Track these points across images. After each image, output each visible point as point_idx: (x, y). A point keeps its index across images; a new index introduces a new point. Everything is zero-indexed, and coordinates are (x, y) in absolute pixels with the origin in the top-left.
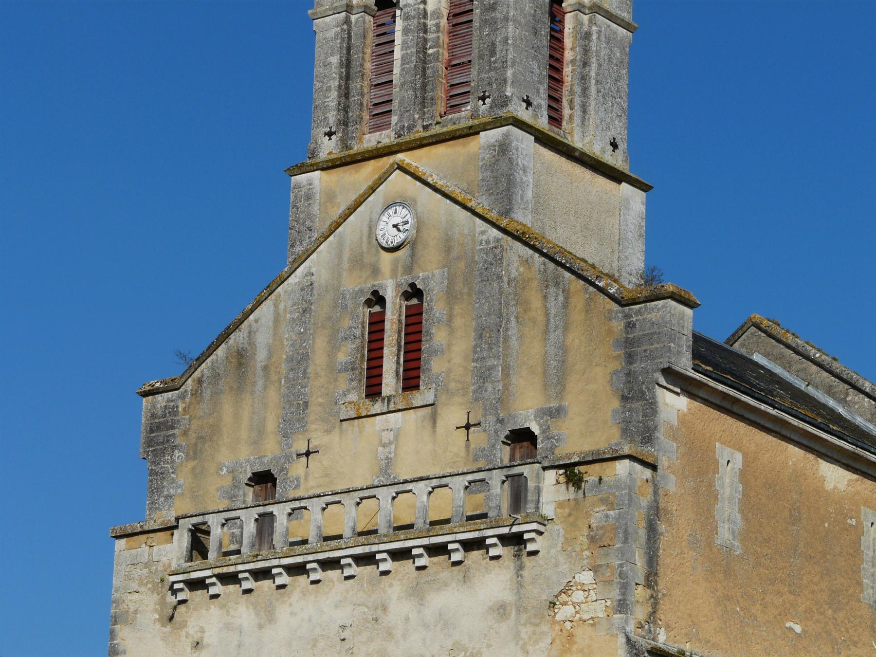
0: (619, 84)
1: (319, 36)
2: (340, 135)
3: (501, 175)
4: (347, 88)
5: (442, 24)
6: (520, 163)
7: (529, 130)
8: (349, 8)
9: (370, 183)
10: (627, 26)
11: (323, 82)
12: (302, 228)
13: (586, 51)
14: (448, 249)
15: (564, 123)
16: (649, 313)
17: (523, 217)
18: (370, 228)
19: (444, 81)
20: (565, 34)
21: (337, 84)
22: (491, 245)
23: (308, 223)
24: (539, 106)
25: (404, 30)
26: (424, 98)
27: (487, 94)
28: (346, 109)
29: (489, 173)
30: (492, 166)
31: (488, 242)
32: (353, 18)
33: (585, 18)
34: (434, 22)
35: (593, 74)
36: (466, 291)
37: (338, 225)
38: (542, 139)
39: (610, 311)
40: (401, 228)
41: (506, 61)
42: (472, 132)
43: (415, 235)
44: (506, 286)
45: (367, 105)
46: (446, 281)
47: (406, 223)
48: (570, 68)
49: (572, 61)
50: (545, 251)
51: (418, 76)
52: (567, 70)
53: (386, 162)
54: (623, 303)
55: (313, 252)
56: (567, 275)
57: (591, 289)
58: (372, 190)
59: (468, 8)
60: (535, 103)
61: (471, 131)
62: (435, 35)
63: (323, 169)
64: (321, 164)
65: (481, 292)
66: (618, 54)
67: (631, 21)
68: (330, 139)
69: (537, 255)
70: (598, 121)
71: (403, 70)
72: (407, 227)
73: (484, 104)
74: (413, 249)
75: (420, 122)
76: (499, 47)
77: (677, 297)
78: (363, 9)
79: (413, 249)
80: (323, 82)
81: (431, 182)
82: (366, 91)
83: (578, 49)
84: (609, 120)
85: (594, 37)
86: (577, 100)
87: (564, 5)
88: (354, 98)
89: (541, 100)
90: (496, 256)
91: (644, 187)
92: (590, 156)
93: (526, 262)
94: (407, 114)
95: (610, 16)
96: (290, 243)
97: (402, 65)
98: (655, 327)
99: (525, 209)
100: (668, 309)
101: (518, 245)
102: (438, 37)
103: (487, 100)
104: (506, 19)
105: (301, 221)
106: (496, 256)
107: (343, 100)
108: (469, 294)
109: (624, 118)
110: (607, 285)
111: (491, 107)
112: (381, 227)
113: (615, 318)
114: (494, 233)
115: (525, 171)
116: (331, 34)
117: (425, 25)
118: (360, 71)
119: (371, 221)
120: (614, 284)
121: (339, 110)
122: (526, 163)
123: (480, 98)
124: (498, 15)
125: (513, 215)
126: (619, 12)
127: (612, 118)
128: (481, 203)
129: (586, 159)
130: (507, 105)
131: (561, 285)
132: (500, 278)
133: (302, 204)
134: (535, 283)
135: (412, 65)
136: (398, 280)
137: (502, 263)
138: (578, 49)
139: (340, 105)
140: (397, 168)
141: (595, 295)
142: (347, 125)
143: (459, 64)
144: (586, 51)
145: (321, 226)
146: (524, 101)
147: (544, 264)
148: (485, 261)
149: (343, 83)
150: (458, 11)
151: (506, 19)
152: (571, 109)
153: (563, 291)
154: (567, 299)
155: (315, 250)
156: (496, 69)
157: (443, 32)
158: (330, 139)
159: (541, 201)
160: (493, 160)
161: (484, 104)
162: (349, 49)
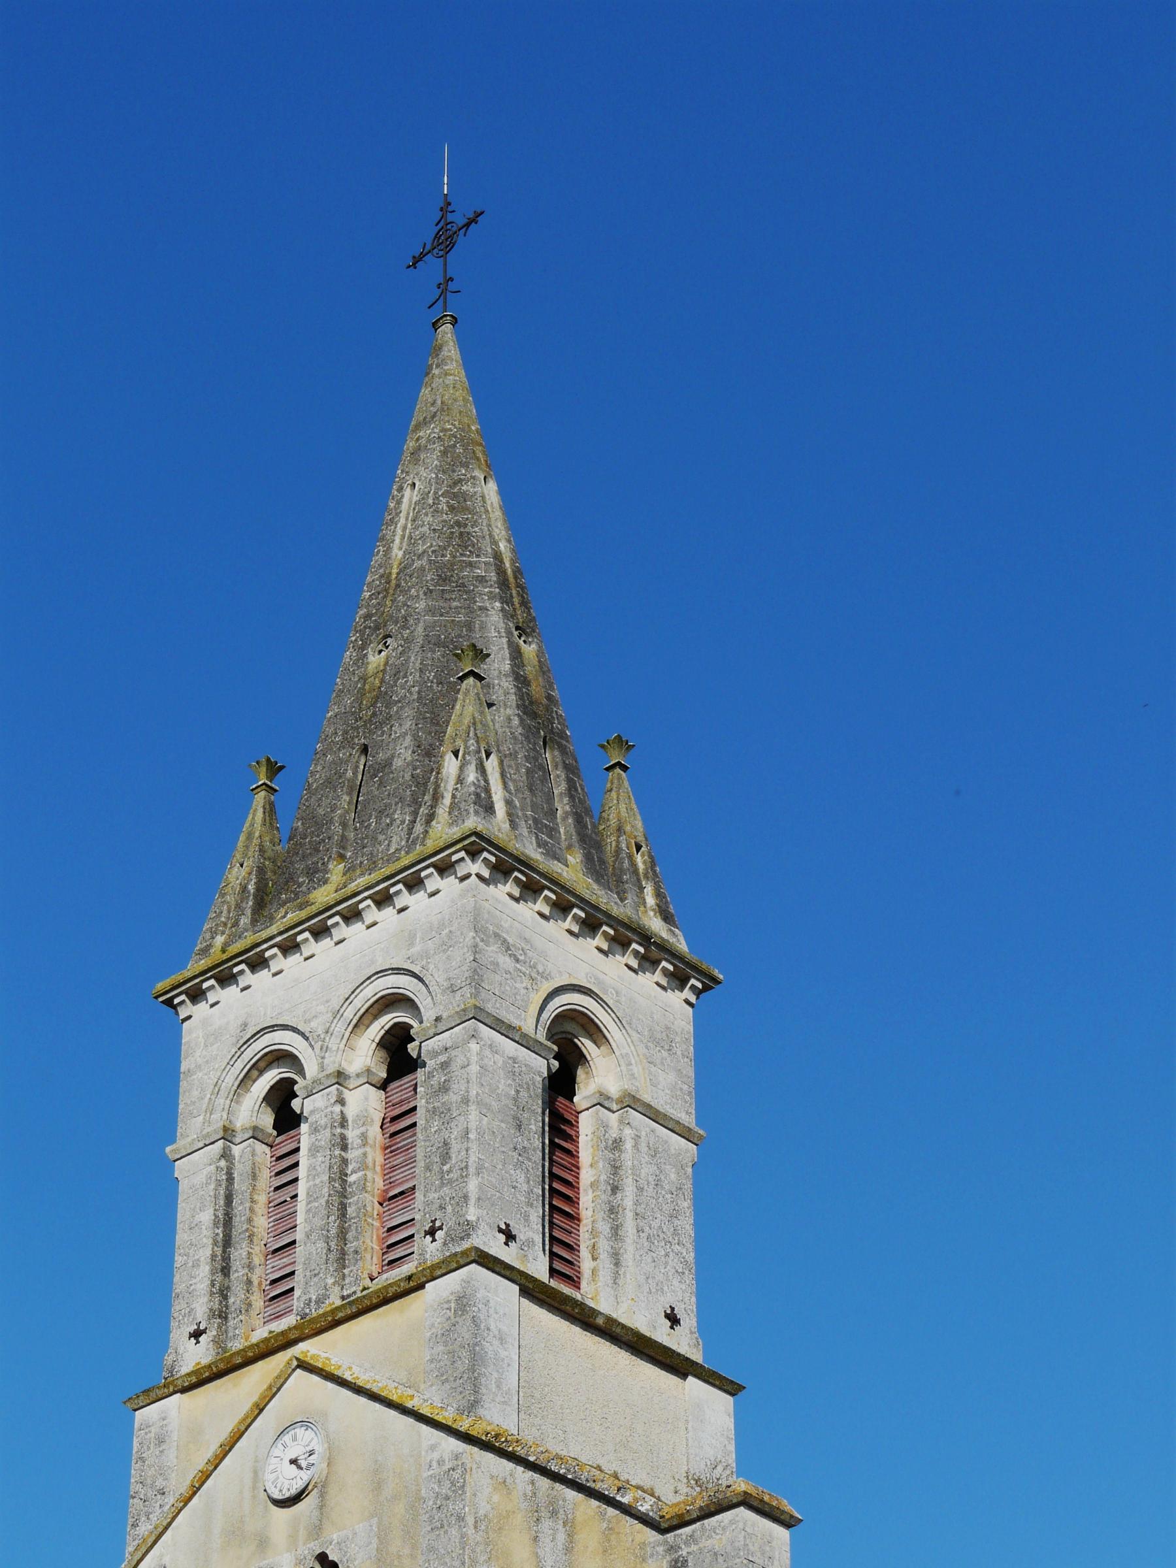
0: (676, 1222)
1: (183, 1186)
2: (214, 1333)
3: (466, 1362)
4: (226, 1258)
5: (371, 1134)
6: (492, 1327)
7: (508, 1273)
8: (228, 1134)
9: (255, 1398)
10: (686, 1134)
11: (187, 1255)
12: (150, 1493)
13: (616, 1168)
14: (378, 1486)
15: (584, 1284)
16: (710, 1537)
17: (497, 1416)
18: (256, 1473)
19: (377, 1224)
20: (580, 1145)
21: (209, 1252)
22: (448, 1466)
23: (160, 1483)
24: (530, 1243)
25: (310, 1150)
26: (343, 1253)
27: (438, 1224)
28: (224, 1293)
29: (441, 1348)
30: (447, 1335)
31: (440, 1462)
32: (236, 1150)
33: (613, 1118)
34: (358, 1132)
35: (629, 1203)
36: (407, 1551)
37: (205, 1476)
38: (531, 1290)
39: (643, 1545)
40: (303, 1464)
41: (467, 1167)
42: (413, 1286)
43: (325, 1472)
44: (470, 1531)
45: (260, 1284)
46: (375, 1541)
47: (311, 1453)
48: (590, 1196)
49: (592, 1185)
50: (532, 1459)
51: (332, 1218)
52: (586, 1200)
53: (280, 1360)
54: (664, 1525)
55: (166, 1528)
56: (571, 1494)
57: (611, 1512)
58: (260, 1409)
59: (411, 1105)
60: (521, 1237)
61: (412, 1284)
62: (361, 1151)
63: (184, 1390)
64: (179, 1382)
65: (431, 1549)
66: (673, 1176)
67: (693, 1125)
68: (198, 1342)
69: (520, 1469)
70: (642, 1279)
71: (308, 1211)
72: (312, 1459)
73: (434, 1240)
74: (322, 1495)
75: (337, 1289)
76: (455, 1147)
77: (755, 1504)
78: (250, 1134)
79: (322, 1495)
80: (187, 1255)
81: (349, 1378)
82: (257, 1260)
83: (601, 1165)
84: (660, 1277)
85: (628, 1145)
86: (604, 1246)
87: (575, 1099)
88: (238, 1273)
89: (532, 1230)
90: (455, 1482)
91: (731, 1388)
92: (624, 1326)
93: (503, 1484)
94: (316, 1279)
95: (655, 1116)
96: (131, 1521)
97: (308, 1204)
98: (720, 1560)
99: (505, 1403)
100: (741, 1525)
101: (490, 1457)
102: (365, 1154)
103: (439, 1235)
104: (466, 1101)
105: (149, 1481)
106: (455, 1482)
107: (219, 1277)
108: (413, 1557)
109: (689, 1278)
110: (636, 1500)
111: (445, 1244)
112: (272, 1467)
113: (652, 1555)
114: (453, 1444)
115: (502, 1340)
116: (201, 1178)
117: (343, 1138)
118: (247, 1230)
119: (256, 1461)
120: (648, 1497)
121: (212, 1294)
122: (505, 1329)
123: (427, 1233)
124: (453, 1097)
125: (481, 1412)
126: (671, 1111)
127: (666, 1274)
128: (427, 1400)
129: (618, 1330)
130: (469, 1235)
131: (561, 1515)
132: (461, 1518)
133: (150, 1455)
134: (519, 1519)
135: (323, 1201)
136: (299, 1552)
137: (464, 1492)
138: (601, 1165)
139: (213, 1285)
140: (298, 1366)
141: (618, 1522)
142: (226, 1318)
143: (402, 1193)
144: (616, 1168)
145: (179, 1484)
146: (500, 1231)
147: (533, 1483)
148: (438, 1495)
149: (219, 1251)
150: (397, 1112)
151: (466, 1101)
152: (594, 1259)
153: (565, 1524)
154: (570, 1536)
155: (170, 1524)
156: (450, 1182)
157: (373, 1146)
158: (198, 1342)
159: (537, 1395)
160: (447, 1326)
161: (434, 1240)
162: (229, 1199)
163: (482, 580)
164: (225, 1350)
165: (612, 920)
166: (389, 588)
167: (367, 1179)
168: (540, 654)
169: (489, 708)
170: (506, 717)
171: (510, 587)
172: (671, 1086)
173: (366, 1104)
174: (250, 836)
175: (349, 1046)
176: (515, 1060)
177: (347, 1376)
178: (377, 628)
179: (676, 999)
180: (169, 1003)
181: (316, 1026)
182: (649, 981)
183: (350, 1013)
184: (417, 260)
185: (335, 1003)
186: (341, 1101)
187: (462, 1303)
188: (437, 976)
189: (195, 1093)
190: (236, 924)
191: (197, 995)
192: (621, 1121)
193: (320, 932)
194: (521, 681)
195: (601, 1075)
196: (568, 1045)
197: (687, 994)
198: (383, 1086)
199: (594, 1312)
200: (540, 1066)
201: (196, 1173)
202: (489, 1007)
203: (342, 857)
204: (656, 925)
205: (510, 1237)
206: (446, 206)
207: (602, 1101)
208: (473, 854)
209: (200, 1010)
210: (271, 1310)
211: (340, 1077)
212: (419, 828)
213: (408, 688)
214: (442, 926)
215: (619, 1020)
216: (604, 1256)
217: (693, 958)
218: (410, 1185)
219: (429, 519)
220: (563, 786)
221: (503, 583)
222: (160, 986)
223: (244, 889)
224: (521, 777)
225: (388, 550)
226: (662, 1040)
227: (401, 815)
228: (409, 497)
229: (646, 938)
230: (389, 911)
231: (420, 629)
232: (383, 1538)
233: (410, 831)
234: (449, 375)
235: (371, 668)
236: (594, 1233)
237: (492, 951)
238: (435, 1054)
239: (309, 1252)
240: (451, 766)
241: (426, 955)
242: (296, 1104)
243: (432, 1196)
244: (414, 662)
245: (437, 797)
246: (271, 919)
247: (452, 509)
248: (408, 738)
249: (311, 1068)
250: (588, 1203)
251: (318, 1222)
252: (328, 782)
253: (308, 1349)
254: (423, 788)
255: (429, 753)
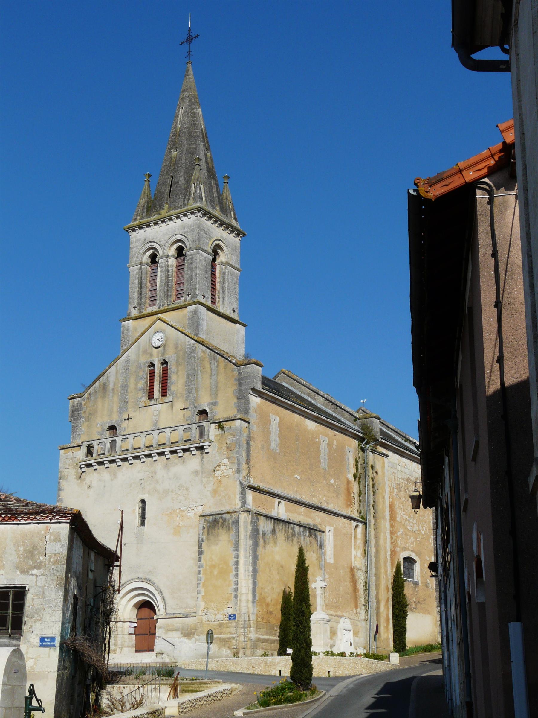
1: (131, 273)
4: (141, 291)
10: (238, 270)
13: (224, 278)
14: (176, 348)
15: (216, 303)
17: (203, 336)
23: (128, 339)
24: (208, 298)
30: (191, 318)
31: (190, 345)
32: (143, 267)
33: (224, 267)
35: (226, 286)
38: (209, 309)
39: (233, 368)
42: (184, 307)
58: (150, 327)
63: (133, 320)
65: (188, 362)
74: (164, 347)
76: (194, 277)
79: (164, 347)
85: (227, 273)
86: (221, 296)
88: (143, 295)
89: (209, 295)
90: (193, 350)
91: (244, 325)
93: (204, 352)
95: (232, 266)
104: (196, 267)
106: (193, 350)
109: (237, 302)
116: (135, 273)
117: (168, 269)
128: (188, 331)
133: (125, 332)
134: (207, 359)
144: (224, 278)
145: (132, 339)
151: (196, 267)
163: (198, 136)
164: (141, 312)
165: (226, 224)
166: (176, 135)
167: (173, 279)
168: (211, 154)
169: (200, 173)
170: (205, 172)
171: (205, 138)
172: (234, 260)
173: (172, 262)
174: (144, 193)
175: (170, 249)
176: (206, 257)
177: (170, 323)
178: (174, 145)
179: (237, 239)
180: (127, 231)
181: (162, 243)
182: (232, 236)
183: (170, 242)
184: (182, 43)
185: (167, 239)
186: (168, 261)
187: (195, 312)
188: (190, 238)
189: (133, 253)
190: (142, 215)
191: (134, 230)
192: (225, 268)
193: (163, 222)
194: (207, 163)
195: (222, 258)
196: (216, 251)
197: (239, 238)
198: (176, 258)
199: (220, 312)
200: (211, 258)
201: (134, 270)
202: (202, 247)
203: (167, 203)
204: (234, 223)
205: (204, 297)
206: (190, 31)
207: (222, 263)
208: (199, 211)
209: (134, 234)
210: (150, 303)
211: (168, 256)
212: (186, 202)
213: (183, 163)
214: (191, 226)
215: (226, 246)
216: (221, 298)
217: (241, 230)
218: (182, 281)
219: (186, 119)
220: (215, 190)
221: (203, 137)
222: (125, 227)
223: (144, 206)
224: (207, 189)
225: (176, 124)
226: (234, 249)
227: (182, 197)
228: (181, 111)
229: (232, 227)
230: (179, 220)
231: (185, 149)
232: (178, 358)
233: (184, 202)
234: (191, 79)
235: (173, 155)
236: (219, 292)
237: (202, 233)
238: (189, 255)
239: (159, 293)
240: (193, 187)
241: (187, 232)
242: (157, 260)
243: (189, 287)
244: (184, 157)
245: (190, 195)
246: (151, 216)
247: (192, 116)
248: (183, 178)
249: (161, 253)
250: (218, 285)
251: (163, 288)
252: (163, 183)
253: (160, 315)
254: (187, 191)
255: (188, 181)
